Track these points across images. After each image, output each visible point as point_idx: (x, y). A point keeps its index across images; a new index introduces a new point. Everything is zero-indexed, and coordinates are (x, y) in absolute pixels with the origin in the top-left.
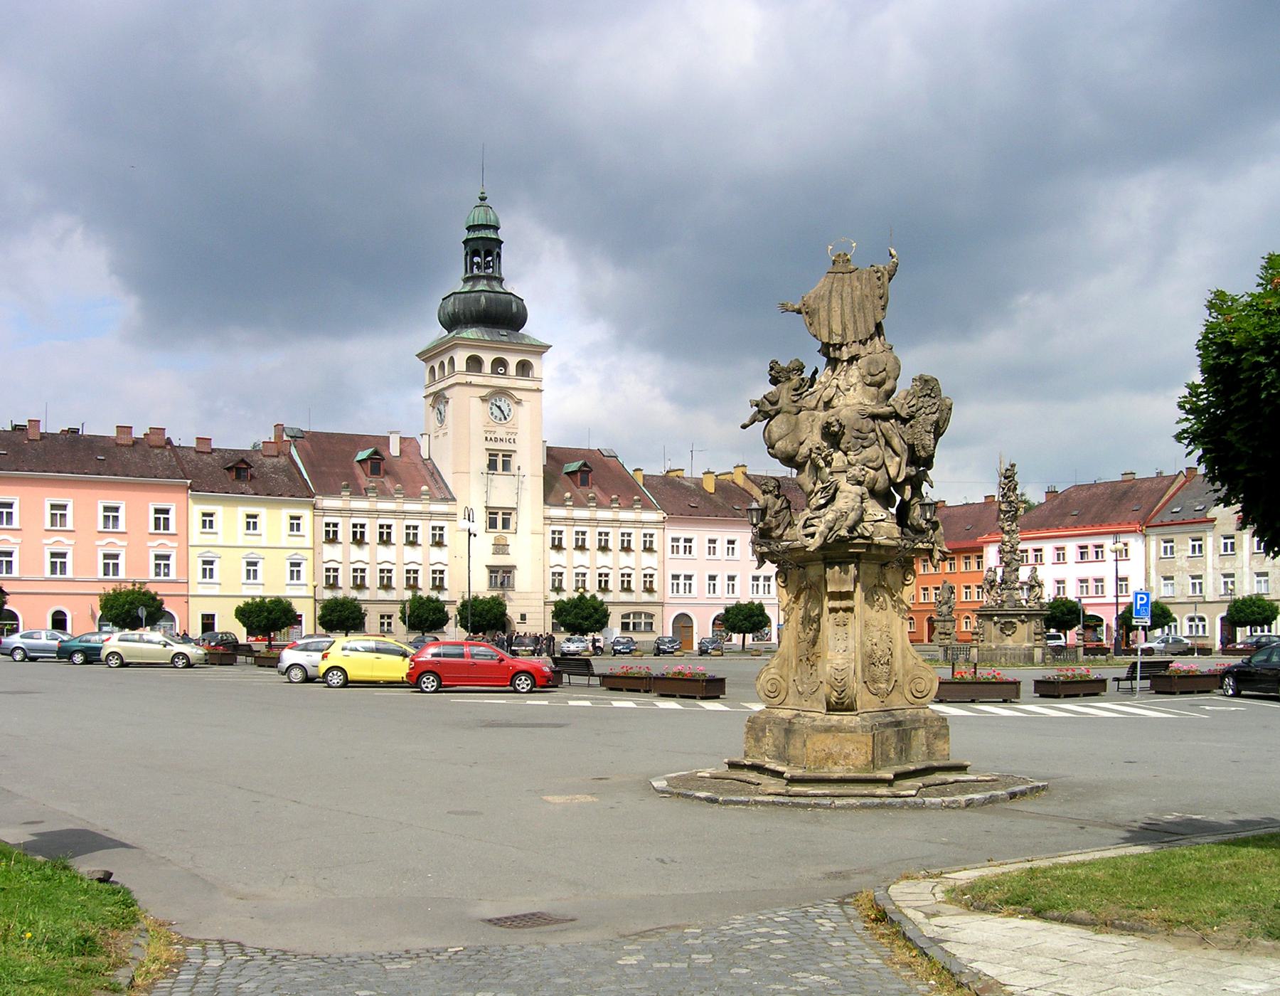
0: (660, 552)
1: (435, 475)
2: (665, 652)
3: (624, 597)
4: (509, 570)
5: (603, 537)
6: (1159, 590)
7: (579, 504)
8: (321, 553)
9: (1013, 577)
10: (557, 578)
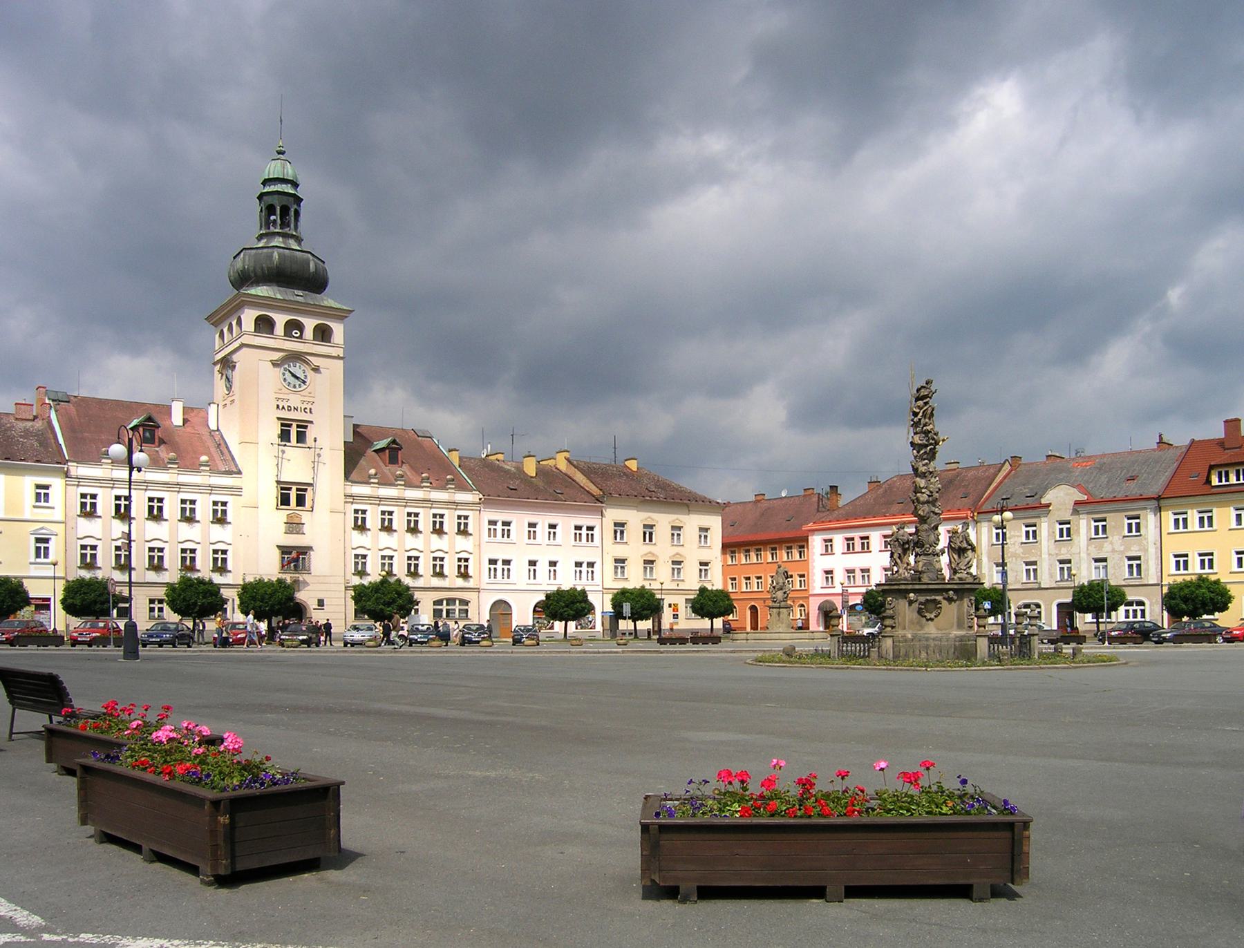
1: (222, 446)
2: (470, 642)
3: (436, 582)
4: (304, 551)
6: (991, 576)
7: (384, 483)
9: (932, 538)
10: (360, 561)
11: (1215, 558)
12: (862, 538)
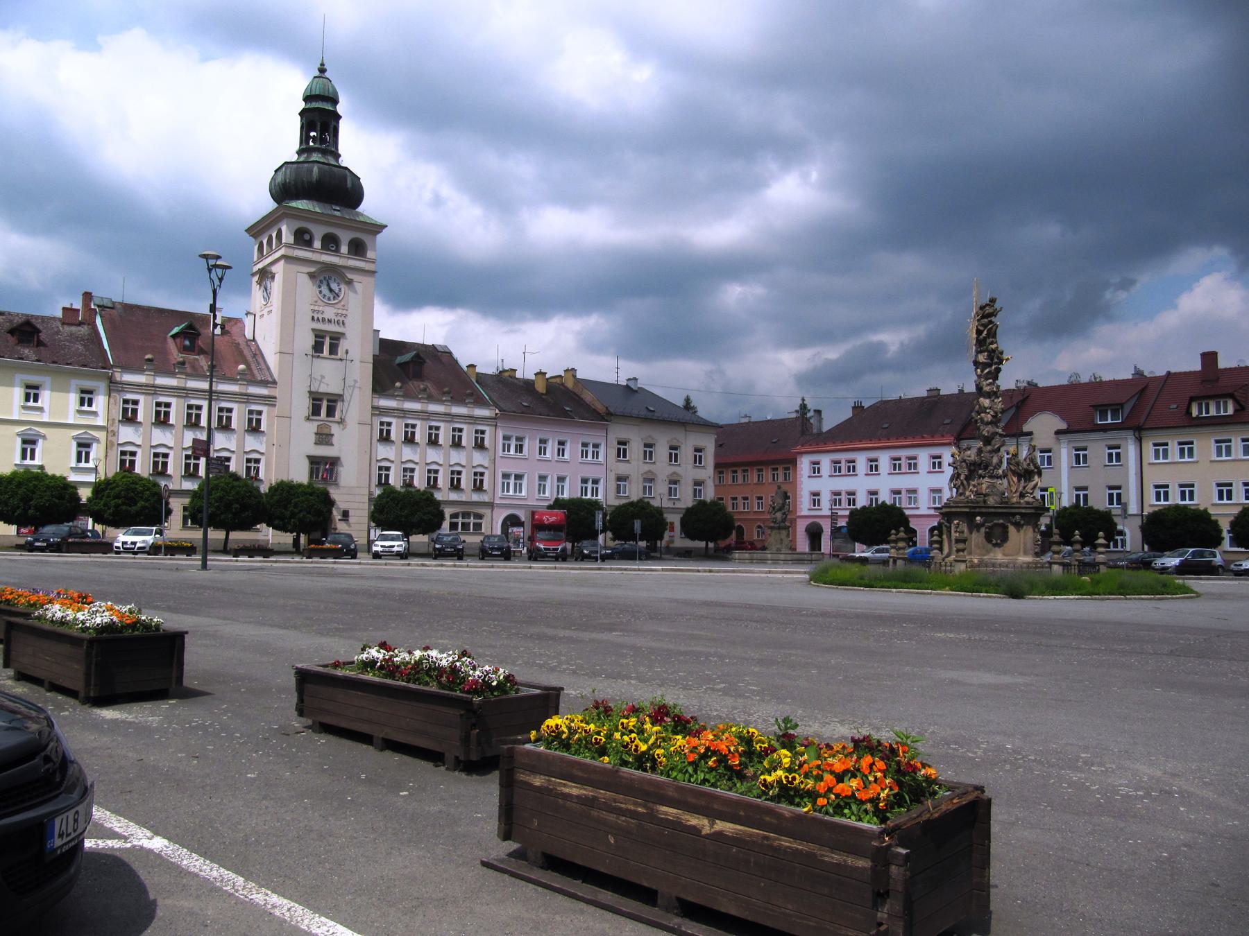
0: (492, 451)
3: (454, 496)
4: (334, 462)
5: (434, 431)
8: (114, 434)
9: (995, 460)
11: (1195, 489)
12: (910, 458)
